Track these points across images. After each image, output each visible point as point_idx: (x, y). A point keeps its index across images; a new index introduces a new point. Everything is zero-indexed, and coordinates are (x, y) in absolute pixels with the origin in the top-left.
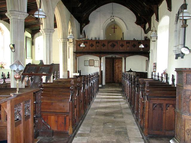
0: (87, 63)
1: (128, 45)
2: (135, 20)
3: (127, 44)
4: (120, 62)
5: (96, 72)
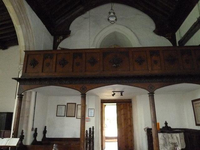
0: (62, 111)
1: (154, 58)
2: (153, 27)
3: (151, 55)
4: (128, 108)
5: (90, 129)
